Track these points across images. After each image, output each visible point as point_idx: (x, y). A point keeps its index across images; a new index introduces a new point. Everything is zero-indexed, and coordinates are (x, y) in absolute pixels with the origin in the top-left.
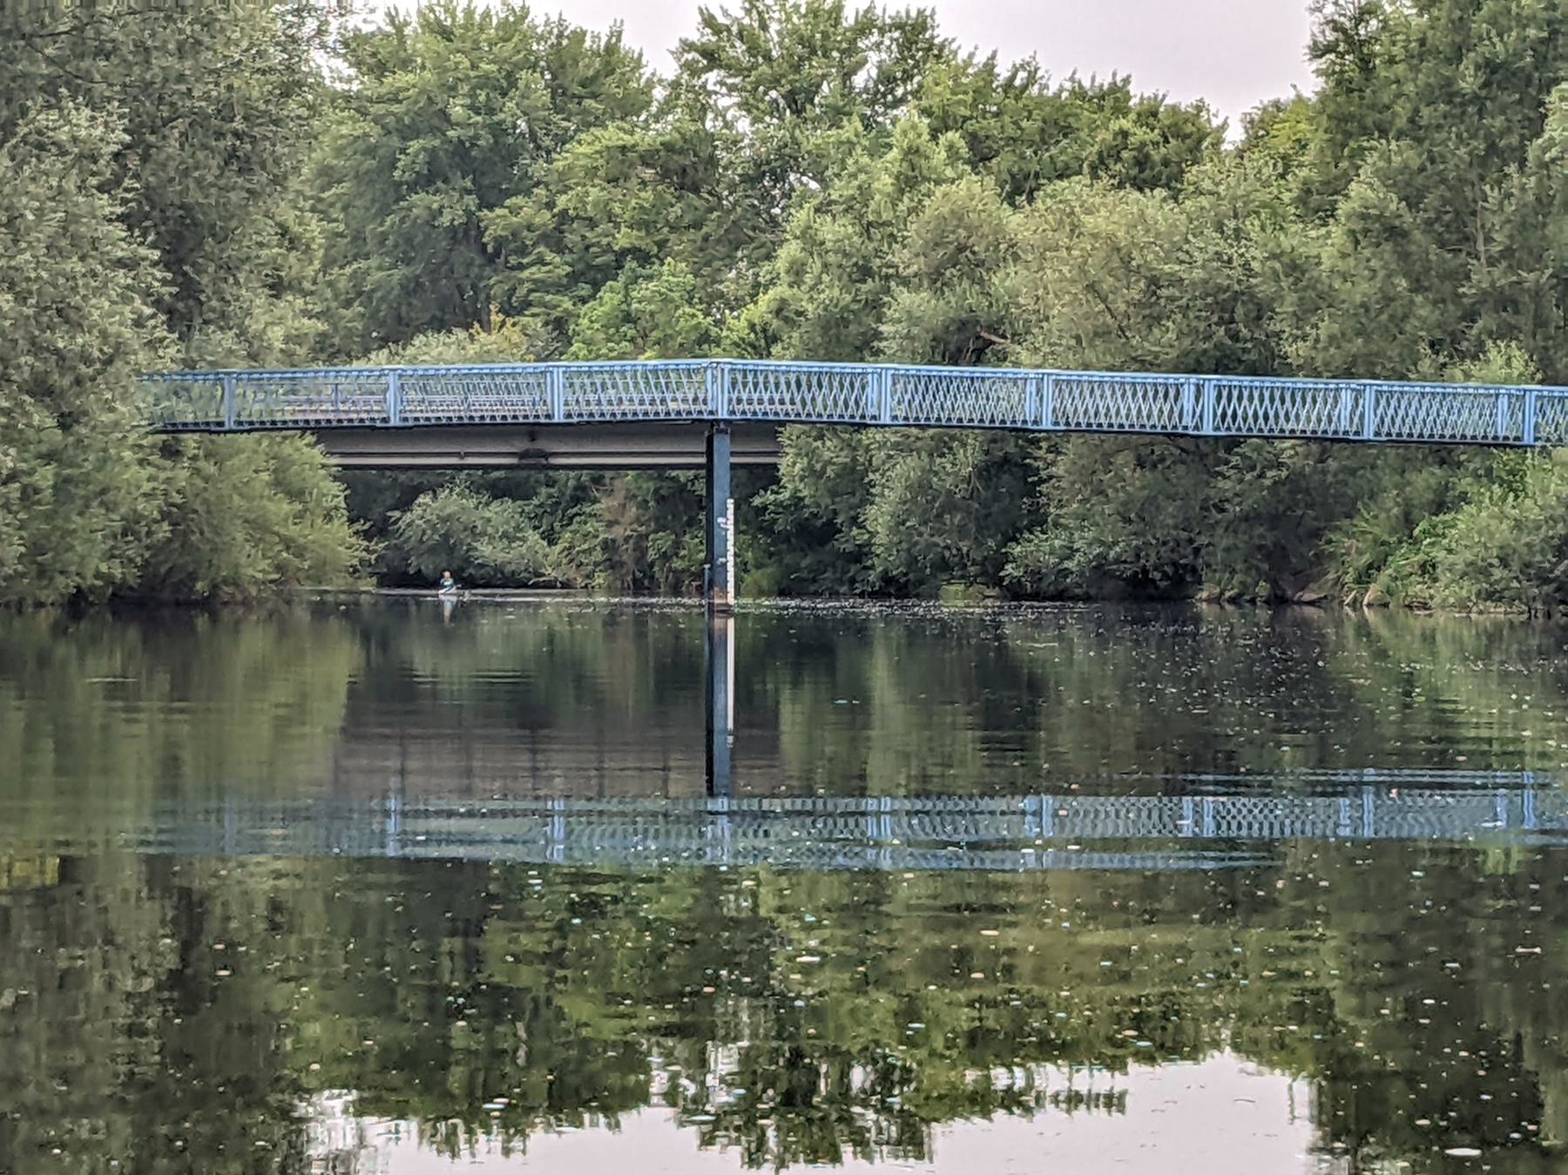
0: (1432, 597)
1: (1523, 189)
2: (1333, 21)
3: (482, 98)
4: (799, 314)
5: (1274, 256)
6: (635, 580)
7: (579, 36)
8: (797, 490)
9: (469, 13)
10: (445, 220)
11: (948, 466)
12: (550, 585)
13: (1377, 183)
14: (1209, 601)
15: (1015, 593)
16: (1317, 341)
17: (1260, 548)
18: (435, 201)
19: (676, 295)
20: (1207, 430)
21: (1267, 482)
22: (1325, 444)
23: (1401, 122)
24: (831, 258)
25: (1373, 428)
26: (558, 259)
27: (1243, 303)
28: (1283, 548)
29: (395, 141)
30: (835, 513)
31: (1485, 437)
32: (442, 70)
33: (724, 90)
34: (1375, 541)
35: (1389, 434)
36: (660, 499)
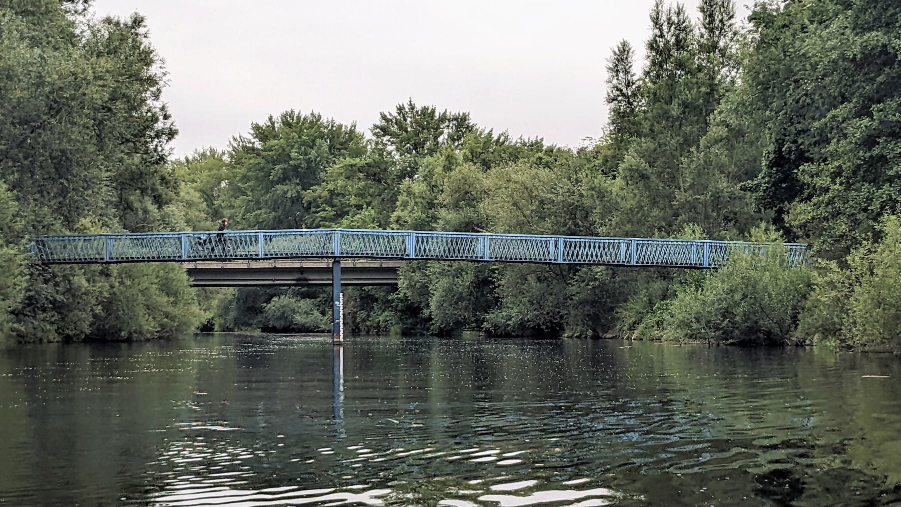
0: (662, 336)
1: (698, 158)
2: (616, 87)
3: (303, 149)
4: (405, 222)
5: (593, 189)
6: (353, 329)
7: (340, 126)
8: (405, 294)
9: (299, 118)
10: (289, 195)
11: (460, 282)
12: (323, 331)
13: (635, 155)
14: (568, 337)
15: (489, 335)
16: (611, 225)
17: (588, 315)
18: (286, 188)
19: (367, 220)
20: (560, 261)
21: (590, 287)
22: (615, 267)
23: (646, 130)
24: (418, 200)
25: (636, 260)
26: (330, 209)
27: (580, 210)
28: (597, 314)
29: (270, 166)
30: (421, 302)
31: (686, 264)
32: (287, 139)
33: (390, 143)
34: (637, 312)
35: (643, 263)
36: (361, 298)
